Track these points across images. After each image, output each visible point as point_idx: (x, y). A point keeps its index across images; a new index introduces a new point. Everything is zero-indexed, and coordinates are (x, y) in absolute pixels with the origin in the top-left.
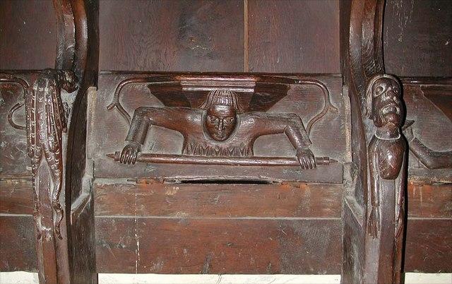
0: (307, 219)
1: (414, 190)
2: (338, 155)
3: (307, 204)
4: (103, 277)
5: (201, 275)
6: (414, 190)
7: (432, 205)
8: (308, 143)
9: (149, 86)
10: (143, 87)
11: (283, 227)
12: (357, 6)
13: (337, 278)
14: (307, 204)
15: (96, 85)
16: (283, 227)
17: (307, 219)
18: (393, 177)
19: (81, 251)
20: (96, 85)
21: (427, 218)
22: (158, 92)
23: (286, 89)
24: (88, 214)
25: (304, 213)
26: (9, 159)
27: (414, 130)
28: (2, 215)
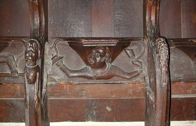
0: (20, 99)
1: (65, 86)
2: (150, 70)
3: (18, 93)
4: (50, 123)
5: (96, 122)
6: (65, 86)
7: (73, 93)
8: (15, 67)
9: (68, 43)
10: (66, 42)
11: (9, 102)
12: (150, 3)
13: (143, 123)
14: (18, 93)
15: (48, 41)
16: (9, 102)
17: (20, 99)
18: (32, 82)
19: (41, 113)
20: (48, 41)
21: (71, 99)
22: (71, 45)
23: (7, 43)
24: (45, 99)
25: (18, 97)
26: (7, 75)
27: (63, 61)
28: (1, 99)
